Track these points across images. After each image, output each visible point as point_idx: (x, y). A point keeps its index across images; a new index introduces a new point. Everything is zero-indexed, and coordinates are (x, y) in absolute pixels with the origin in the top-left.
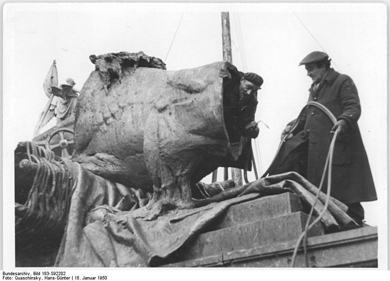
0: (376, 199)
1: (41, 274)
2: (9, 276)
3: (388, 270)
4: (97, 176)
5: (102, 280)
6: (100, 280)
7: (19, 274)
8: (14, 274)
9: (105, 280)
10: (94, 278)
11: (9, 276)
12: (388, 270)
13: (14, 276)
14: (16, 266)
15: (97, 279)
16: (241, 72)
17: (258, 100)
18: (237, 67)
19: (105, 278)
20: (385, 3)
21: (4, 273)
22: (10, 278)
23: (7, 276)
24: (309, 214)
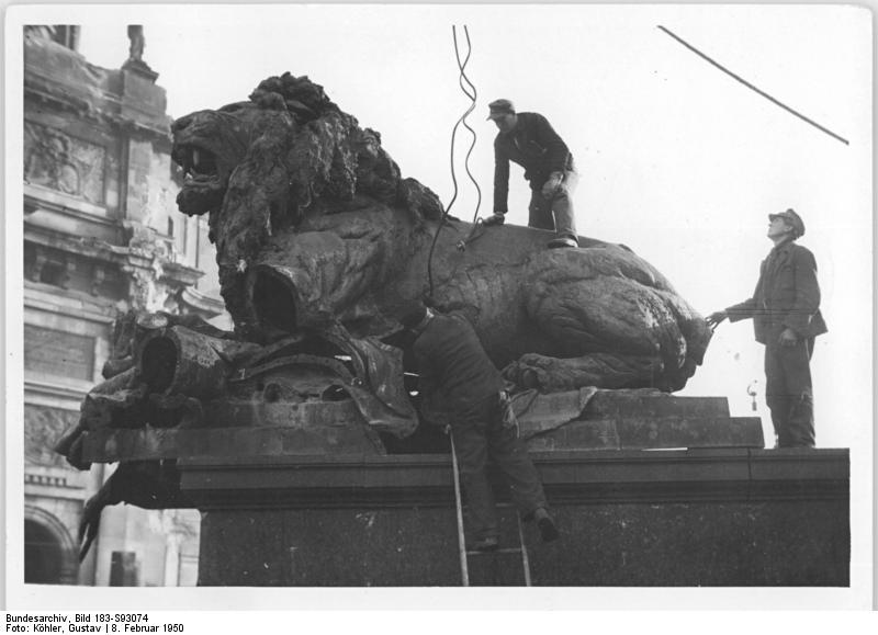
0: (726, 399)
1: (93, 618)
2: (21, 624)
3: (875, 608)
4: (119, 341)
5: (173, 633)
6: (167, 633)
7: (43, 619)
8: (31, 619)
9: (178, 633)
10: (154, 629)
11: (21, 624)
12: (875, 608)
13: (30, 625)
14: (845, 582)
15: (161, 631)
16: (220, 275)
17: (530, 191)
18: (546, 117)
19: (180, 628)
20: (871, 8)
21: (8, 618)
22: (23, 629)
23: (15, 624)
24: (450, 452)
